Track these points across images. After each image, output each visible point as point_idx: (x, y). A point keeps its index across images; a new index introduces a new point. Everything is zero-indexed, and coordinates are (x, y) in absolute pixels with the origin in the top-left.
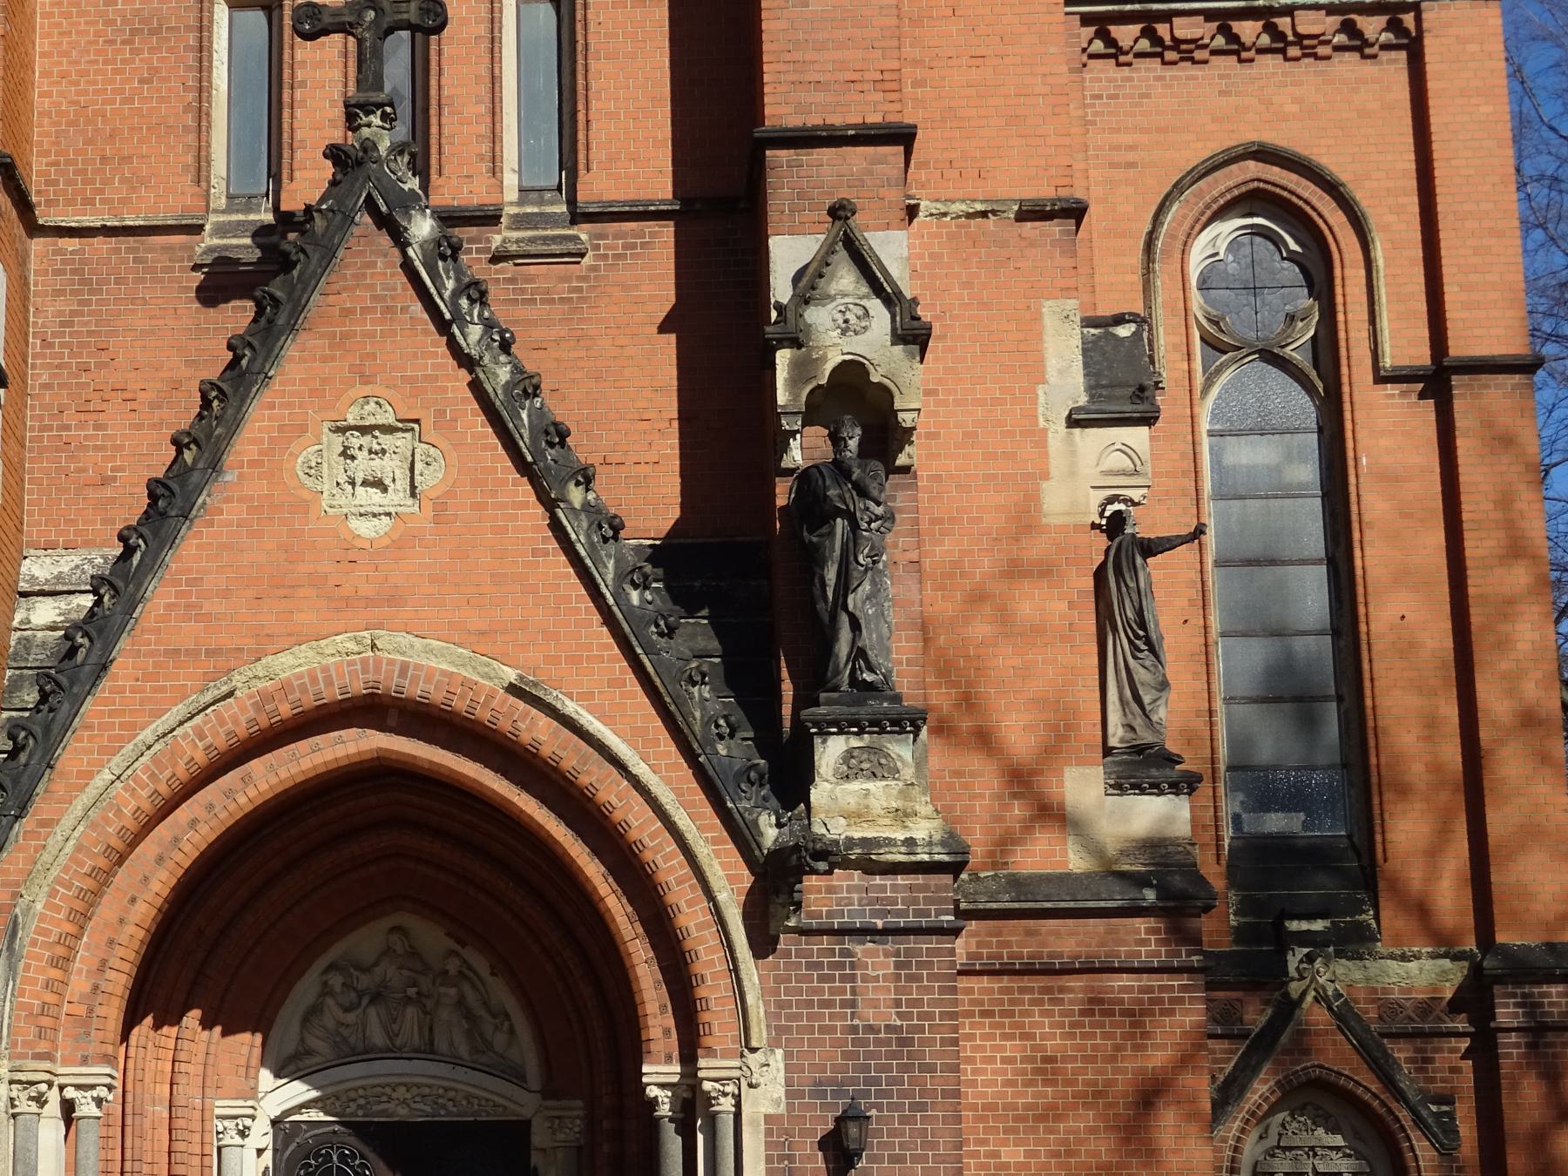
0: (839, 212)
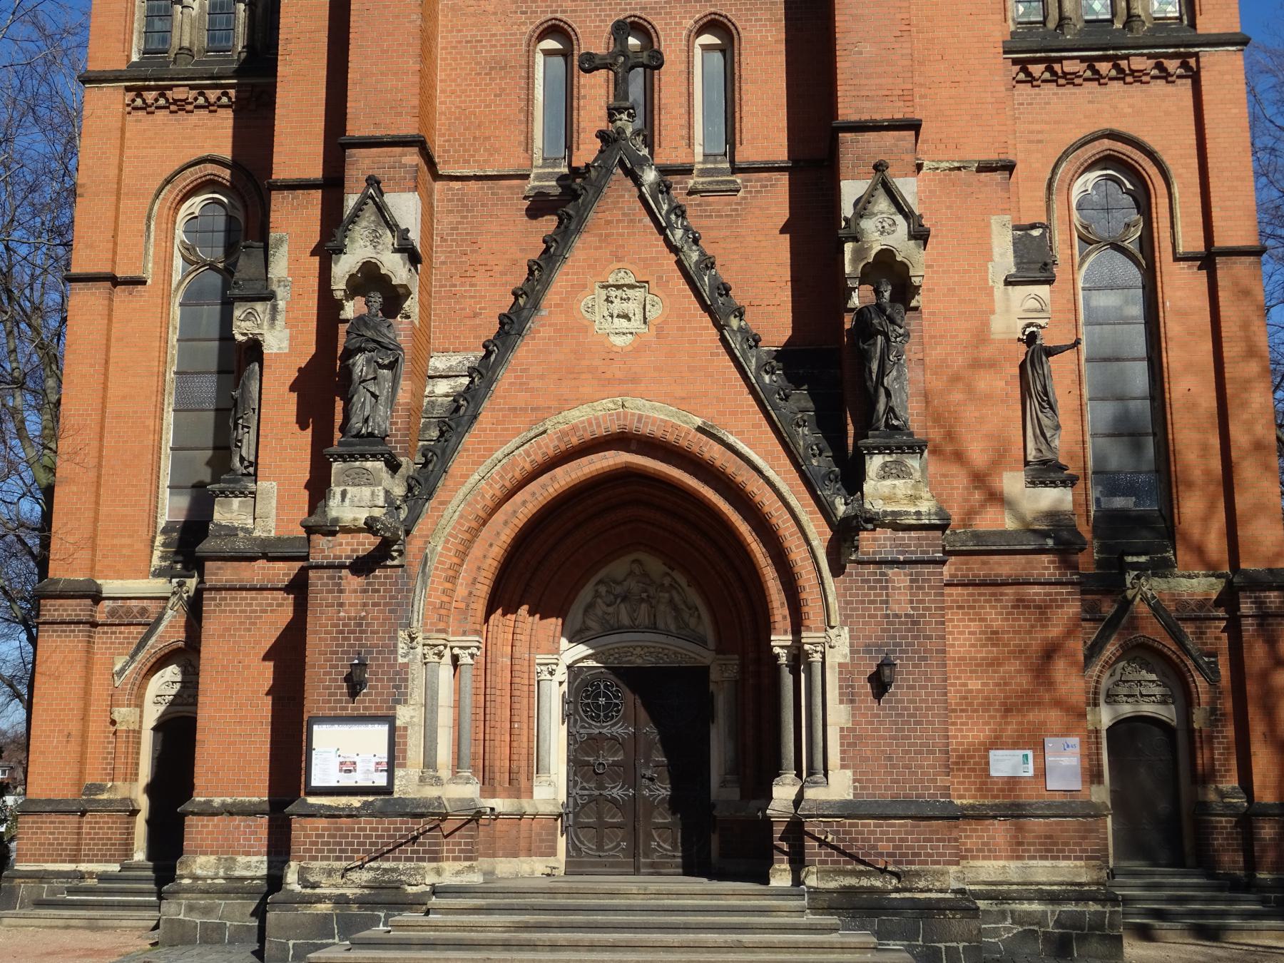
0: (879, 167)
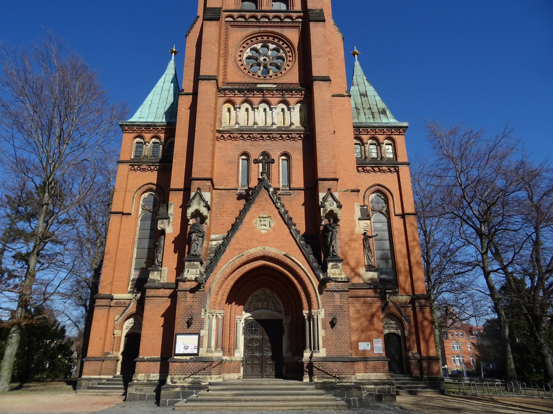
0: (329, 189)
